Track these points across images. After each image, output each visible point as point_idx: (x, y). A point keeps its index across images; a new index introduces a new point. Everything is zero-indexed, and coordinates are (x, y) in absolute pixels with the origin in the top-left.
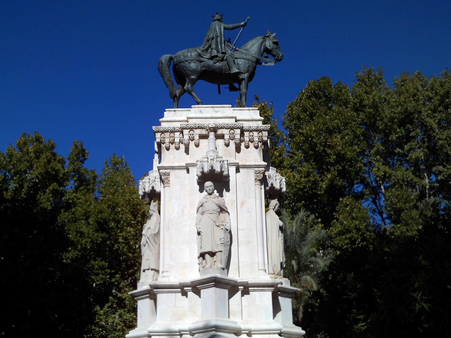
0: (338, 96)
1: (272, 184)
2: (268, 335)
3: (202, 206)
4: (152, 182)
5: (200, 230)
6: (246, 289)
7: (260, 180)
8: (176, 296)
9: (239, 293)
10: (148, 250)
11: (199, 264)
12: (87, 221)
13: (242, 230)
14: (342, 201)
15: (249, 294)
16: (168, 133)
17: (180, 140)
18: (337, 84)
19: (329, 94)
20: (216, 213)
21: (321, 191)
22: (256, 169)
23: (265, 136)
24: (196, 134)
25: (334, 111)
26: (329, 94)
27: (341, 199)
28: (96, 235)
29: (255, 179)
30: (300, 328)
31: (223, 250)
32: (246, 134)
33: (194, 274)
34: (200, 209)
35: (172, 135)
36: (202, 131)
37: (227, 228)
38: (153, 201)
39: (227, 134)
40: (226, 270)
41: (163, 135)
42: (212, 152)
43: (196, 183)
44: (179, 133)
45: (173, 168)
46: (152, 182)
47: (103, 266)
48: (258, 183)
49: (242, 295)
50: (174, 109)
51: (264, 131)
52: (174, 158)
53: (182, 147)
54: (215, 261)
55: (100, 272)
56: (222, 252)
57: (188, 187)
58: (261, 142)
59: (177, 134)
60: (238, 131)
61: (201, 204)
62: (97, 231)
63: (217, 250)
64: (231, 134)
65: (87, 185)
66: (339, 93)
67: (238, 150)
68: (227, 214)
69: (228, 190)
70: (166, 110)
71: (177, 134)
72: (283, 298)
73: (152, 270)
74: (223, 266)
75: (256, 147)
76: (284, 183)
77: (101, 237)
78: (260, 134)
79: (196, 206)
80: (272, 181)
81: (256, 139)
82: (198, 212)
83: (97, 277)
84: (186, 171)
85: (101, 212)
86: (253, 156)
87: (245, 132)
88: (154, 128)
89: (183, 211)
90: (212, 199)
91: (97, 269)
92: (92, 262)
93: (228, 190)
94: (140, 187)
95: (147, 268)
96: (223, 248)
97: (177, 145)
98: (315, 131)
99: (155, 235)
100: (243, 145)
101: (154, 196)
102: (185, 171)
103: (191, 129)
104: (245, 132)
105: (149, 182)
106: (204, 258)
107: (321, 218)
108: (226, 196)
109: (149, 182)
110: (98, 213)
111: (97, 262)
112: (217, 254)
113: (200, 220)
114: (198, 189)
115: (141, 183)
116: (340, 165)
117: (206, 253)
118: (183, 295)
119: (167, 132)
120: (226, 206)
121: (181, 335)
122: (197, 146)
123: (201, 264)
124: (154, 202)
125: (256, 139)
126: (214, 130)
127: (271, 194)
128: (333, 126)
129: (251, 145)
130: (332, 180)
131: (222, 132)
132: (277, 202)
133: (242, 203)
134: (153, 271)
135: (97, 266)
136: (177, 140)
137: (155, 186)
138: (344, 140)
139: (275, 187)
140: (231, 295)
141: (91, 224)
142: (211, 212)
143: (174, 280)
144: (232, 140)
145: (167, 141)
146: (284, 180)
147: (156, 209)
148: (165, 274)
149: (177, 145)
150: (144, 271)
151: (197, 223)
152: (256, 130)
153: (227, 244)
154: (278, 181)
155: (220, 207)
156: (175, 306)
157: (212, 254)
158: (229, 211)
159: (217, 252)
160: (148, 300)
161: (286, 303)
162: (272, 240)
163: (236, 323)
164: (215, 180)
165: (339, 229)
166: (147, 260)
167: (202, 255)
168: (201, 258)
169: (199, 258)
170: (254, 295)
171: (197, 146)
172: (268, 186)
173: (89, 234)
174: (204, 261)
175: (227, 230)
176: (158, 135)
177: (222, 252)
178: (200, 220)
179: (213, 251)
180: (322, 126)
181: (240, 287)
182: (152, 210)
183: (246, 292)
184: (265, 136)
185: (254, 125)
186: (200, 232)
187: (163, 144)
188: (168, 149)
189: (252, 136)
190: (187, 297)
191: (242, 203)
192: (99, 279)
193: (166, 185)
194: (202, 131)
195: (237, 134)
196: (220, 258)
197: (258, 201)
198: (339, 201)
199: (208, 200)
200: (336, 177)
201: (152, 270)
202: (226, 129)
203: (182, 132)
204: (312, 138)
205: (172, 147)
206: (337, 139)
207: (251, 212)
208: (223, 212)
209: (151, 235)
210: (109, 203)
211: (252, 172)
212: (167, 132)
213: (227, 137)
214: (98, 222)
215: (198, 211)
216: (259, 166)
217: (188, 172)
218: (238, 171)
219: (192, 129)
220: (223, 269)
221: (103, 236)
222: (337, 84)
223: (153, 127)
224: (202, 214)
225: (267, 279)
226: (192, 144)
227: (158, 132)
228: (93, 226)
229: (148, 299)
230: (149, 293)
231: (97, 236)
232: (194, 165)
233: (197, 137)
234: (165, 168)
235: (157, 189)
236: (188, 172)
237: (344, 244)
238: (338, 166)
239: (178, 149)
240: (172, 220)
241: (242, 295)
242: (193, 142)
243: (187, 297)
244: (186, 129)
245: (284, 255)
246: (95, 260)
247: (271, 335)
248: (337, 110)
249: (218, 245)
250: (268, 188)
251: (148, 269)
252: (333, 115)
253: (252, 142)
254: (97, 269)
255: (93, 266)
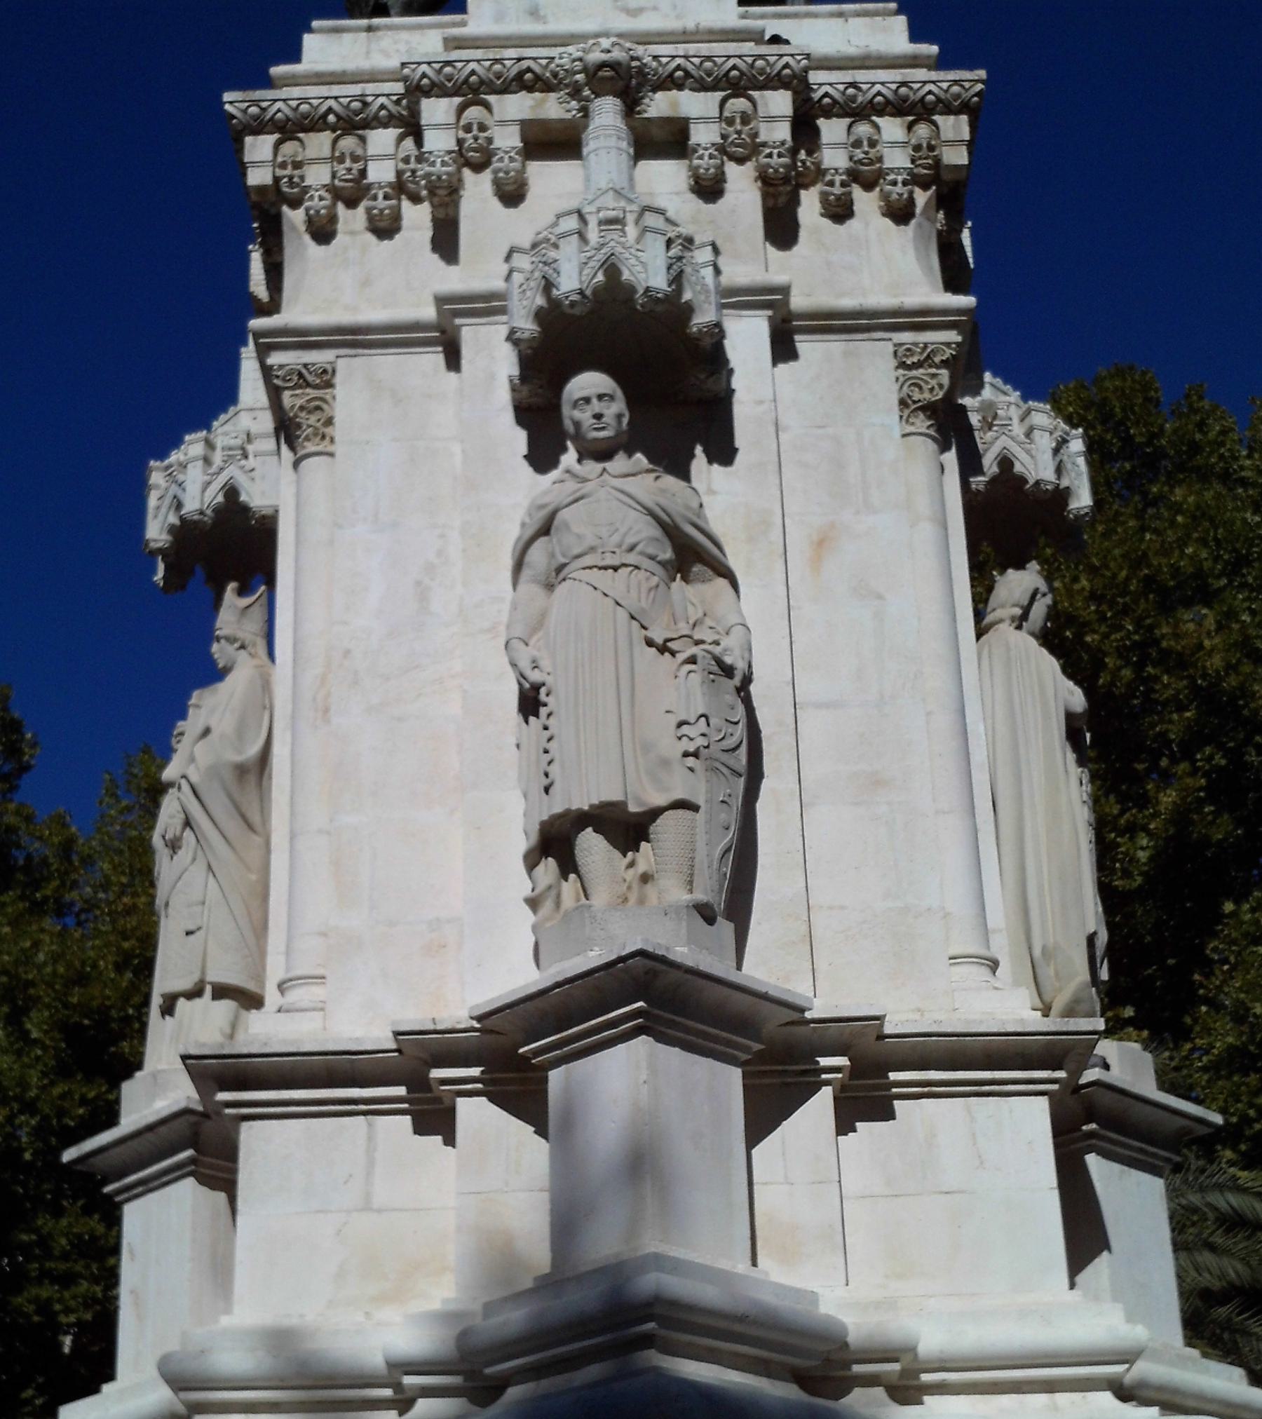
0: (1195, 448)
1: (1006, 463)
2: (1041, 1399)
3: (545, 530)
4: (228, 460)
5: (535, 676)
6: (870, 1075)
7: (929, 409)
8: (370, 1138)
9: (821, 1104)
10: (198, 871)
11: (533, 903)
12: (20, 1024)
13: (819, 706)
14: (1233, 914)
15: (889, 1115)
16: (326, 137)
17: (399, 174)
18: (1188, 396)
19: (1153, 436)
20: (646, 563)
21: (1126, 874)
22: (906, 337)
23: (952, 143)
24: (503, 123)
25: (1177, 508)
26: (1153, 436)
27: (1229, 907)
28: (57, 1091)
29: (903, 403)
30: (1238, 1373)
31: (700, 800)
32: (832, 130)
33: (495, 961)
34: (538, 555)
35: (348, 143)
36: (539, 104)
37: (728, 660)
38: (232, 587)
39: (705, 120)
40: (725, 928)
41: (289, 148)
42: (611, 193)
43: (509, 416)
44: (392, 133)
45: (355, 338)
46: (228, 460)
47: (94, 1238)
48: (922, 423)
49: (844, 1125)
50: (364, 22)
51: (949, 110)
52: (366, 283)
53: (417, 218)
54: (645, 878)
55: (79, 1268)
56: (694, 808)
57: (457, 449)
58: (925, 187)
59: (382, 140)
60: (779, 102)
61: (544, 513)
62: (63, 1071)
63: (660, 800)
64: (730, 122)
65: (36, 885)
66: (1198, 436)
67: (781, 229)
68: (722, 583)
69: (724, 453)
70: (315, 24)
71: (382, 140)
72: (1116, 1167)
73: (221, 992)
74: (708, 889)
75: (900, 213)
76: (1081, 461)
77: (84, 1101)
78: (923, 130)
79: (511, 533)
80: (1004, 441)
81: (897, 160)
82: (526, 573)
83: (67, 1294)
84: (440, 359)
85: (81, 979)
86: (881, 261)
87: (821, 122)
88: (234, 101)
89: (422, 593)
90: (618, 483)
91: (65, 1257)
92: (44, 1221)
93: (724, 453)
94: (152, 501)
95: (186, 984)
96: (702, 787)
97: (381, 203)
98: (1093, 596)
99: (241, 770)
100: (809, 205)
101: (237, 548)
102: (434, 359)
103: (472, 91)
104: (821, 122)
105: (207, 461)
106: (568, 865)
107: (1133, 1005)
108: (711, 492)
109: (207, 461)
110: (70, 983)
111: (64, 1222)
112: (665, 827)
113: (539, 623)
114: (523, 448)
115: (157, 478)
116: (1221, 747)
117: (583, 819)
118: (421, 1128)
119: (313, 123)
120: (716, 527)
121: (404, 1403)
122: (512, 195)
123: (548, 905)
124: (242, 592)
125: (897, 160)
126: (625, 81)
127: (1004, 523)
128: (1176, 571)
129: (866, 202)
130: (1181, 817)
131: (675, 104)
132: (1042, 586)
133: (822, 543)
134: (227, 1005)
135: (63, 1241)
136: (381, 173)
137: (242, 480)
138: (1235, 626)
139: (1022, 480)
140: (764, 1115)
141: (35, 1041)
142: (610, 560)
143: (359, 1019)
144: (740, 161)
145: (317, 176)
146: (1077, 445)
147: (251, 629)
148: (297, 996)
149: (381, 203)
150: (168, 1009)
151: (519, 631)
152: (898, 106)
153: (728, 759)
154: (1045, 443)
155: (671, 530)
156: (367, 1206)
157: (627, 829)
158: (734, 562)
159: (655, 814)
160: (188, 1187)
161: (1134, 1200)
162: (1019, 797)
163: (813, 1297)
164: (636, 375)
165: (1230, 1040)
166: (191, 930)
167: (555, 843)
168: (548, 868)
169: (531, 862)
170: (930, 1123)
171: (512, 195)
172: (982, 473)
173: (23, 1084)
174: (570, 887)
175: (728, 671)
176: (259, 148)
177: (694, 808)
178: (539, 623)
179: (633, 808)
180: (1124, 573)
181: (824, 1061)
182: (231, 640)
183: (864, 1103)
184: (952, 143)
185: (882, 81)
186: (536, 688)
187: (295, 203)
188: (323, 232)
189: (873, 144)
190: (450, 1140)
191: (822, 543)
192: (72, 1303)
193: (311, 447)
194: (539, 104)
195: (772, 119)
196: (682, 857)
197: (926, 532)
198: (1220, 917)
199: (588, 487)
200: (1201, 802)
201: (221, 992)
202: (702, 87)
203: (413, 128)
204: (1083, 627)
205: (352, 220)
206: (1196, 624)
207: (880, 597)
208: (697, 568)
209: (213, 771)
210: (126, 945)
211: (875, 362)
212: (313, 123)
213: (703, 136)
214: (69, 1031)
215: (518, 566)
216: (919, 319)
217: (453, 360)
218: (783, 349)
219: (475, 90)
220: (706, 913)
221: (92, 1094)
222: (1188, 396)
223: (227, 97)
224: (550, 587)
225: (1008, 1008)
226: (477, 192)
227: (259, 126)
228: (45, 1048)
229: (190, 1181)
230: (193, 1141)
231: (63, 1096)
232: (487, 305)
233: (507, 140)
234: (304, 339)
235: (256, 497)
236: (453, 360)
237: (1252, 1113)
238: (1208, 750)
239: (385, 228)
240: (347, 653)
241: (844, 1125)
242: (487, 176)
243: (450, 1140)
244: (437, 89)
245: (1100, 909)
246: (58, 1213)
247: (1063, 1399)
248: (1191, 499)
249: (665, 763)
250: (978, 482)
251: (195, 993)
252: (1173, 523)
253: (868, 186)
254: (65, 1257)
255: (44, 1242)
